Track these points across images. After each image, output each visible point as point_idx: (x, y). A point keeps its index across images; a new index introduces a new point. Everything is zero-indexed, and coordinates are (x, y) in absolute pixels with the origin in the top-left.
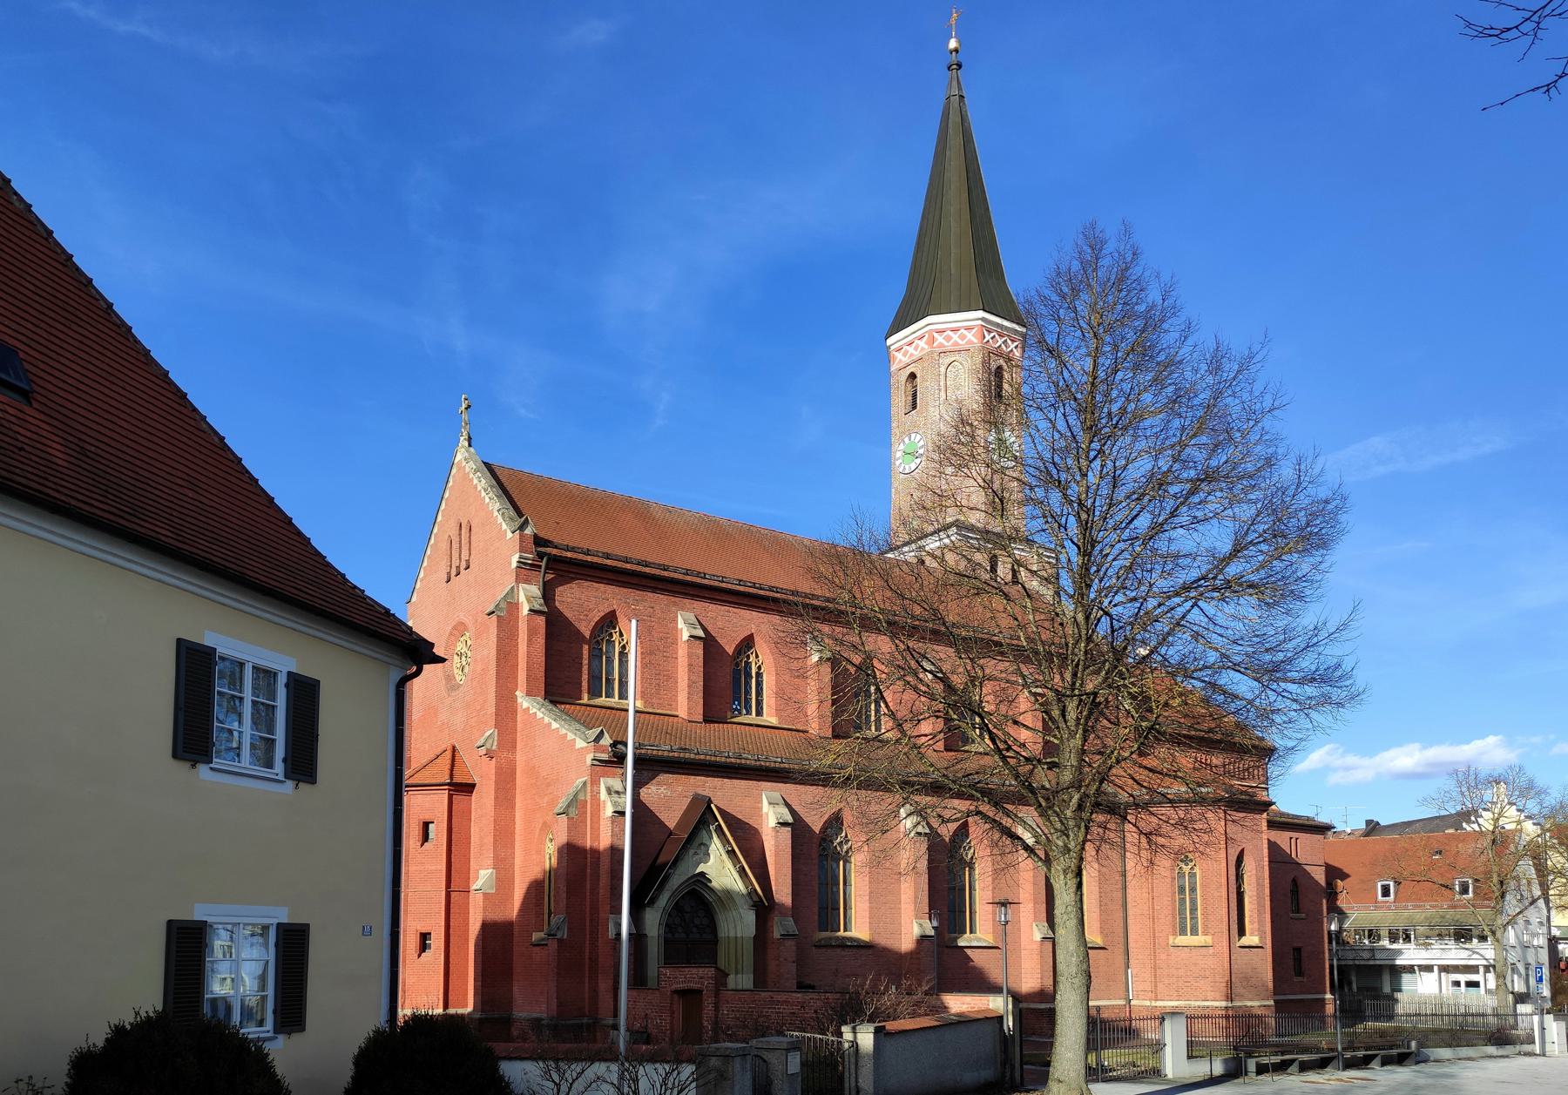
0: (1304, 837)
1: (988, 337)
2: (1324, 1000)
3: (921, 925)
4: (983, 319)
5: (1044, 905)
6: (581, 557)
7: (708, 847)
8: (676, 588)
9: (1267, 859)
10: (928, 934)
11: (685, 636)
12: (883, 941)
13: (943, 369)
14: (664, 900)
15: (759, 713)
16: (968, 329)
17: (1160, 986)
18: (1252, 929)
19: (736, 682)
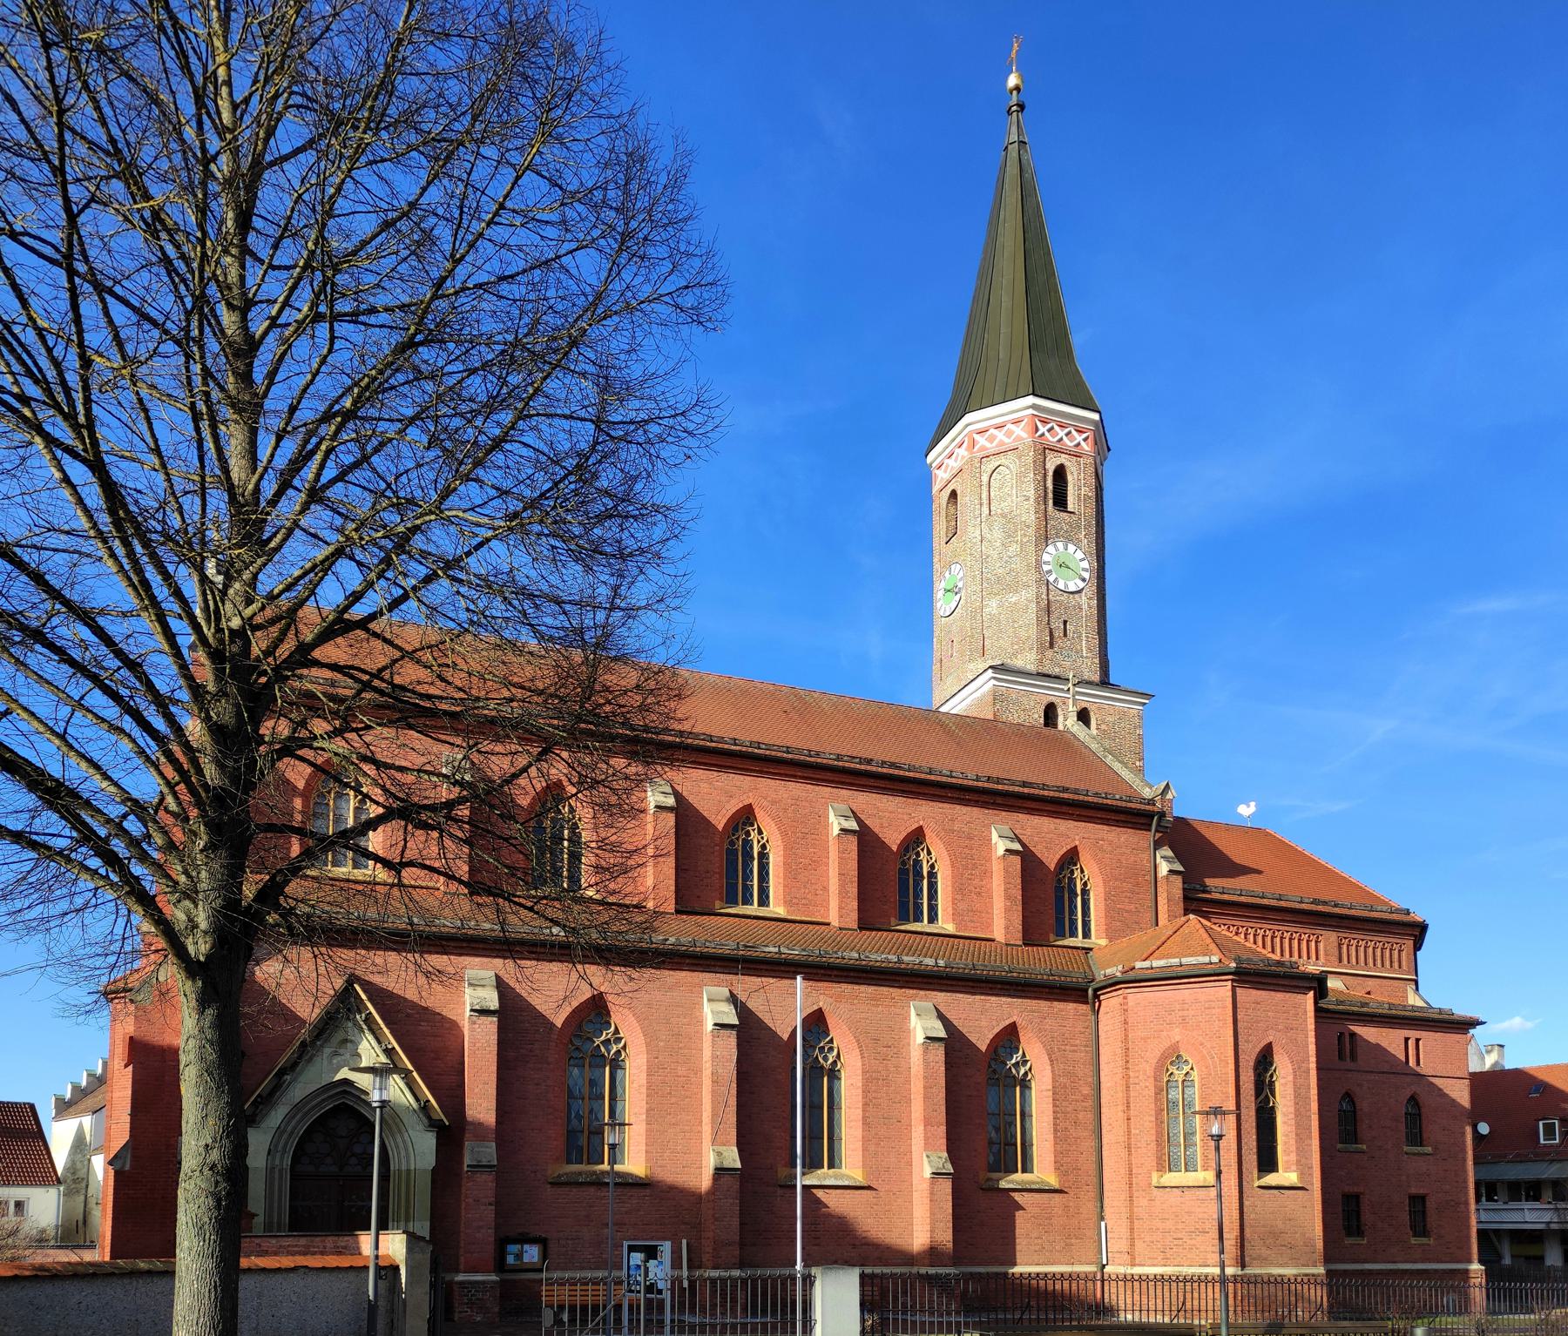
0: (1430, 1039)
1: (1042, 429)
2: (1467, 1271)
3: (719, 1154)
4: (1034, 407)
5: (944, 1128)
6: (1036, 792)
7: (356, 1044)
8: (864, 781)
9: (1313, 1059)
10: (727, 1164)
11: (1001, 851)
12: (671, 1174)
13: (985, 478)
14: (277, 1116)
15: (933, 918)
16: (1017, 422)
17: (1139, 1245)
18: (1287, 1162)
19: (732, 863)
